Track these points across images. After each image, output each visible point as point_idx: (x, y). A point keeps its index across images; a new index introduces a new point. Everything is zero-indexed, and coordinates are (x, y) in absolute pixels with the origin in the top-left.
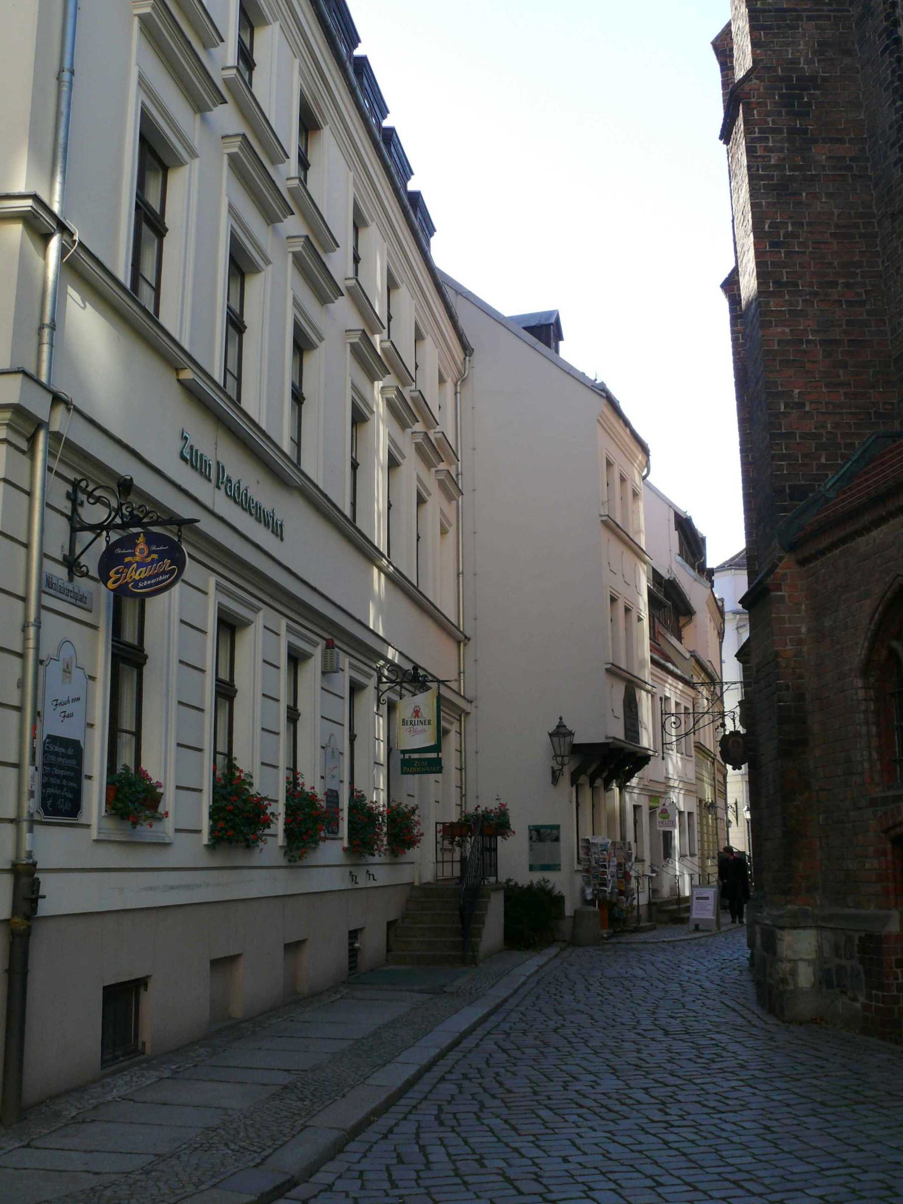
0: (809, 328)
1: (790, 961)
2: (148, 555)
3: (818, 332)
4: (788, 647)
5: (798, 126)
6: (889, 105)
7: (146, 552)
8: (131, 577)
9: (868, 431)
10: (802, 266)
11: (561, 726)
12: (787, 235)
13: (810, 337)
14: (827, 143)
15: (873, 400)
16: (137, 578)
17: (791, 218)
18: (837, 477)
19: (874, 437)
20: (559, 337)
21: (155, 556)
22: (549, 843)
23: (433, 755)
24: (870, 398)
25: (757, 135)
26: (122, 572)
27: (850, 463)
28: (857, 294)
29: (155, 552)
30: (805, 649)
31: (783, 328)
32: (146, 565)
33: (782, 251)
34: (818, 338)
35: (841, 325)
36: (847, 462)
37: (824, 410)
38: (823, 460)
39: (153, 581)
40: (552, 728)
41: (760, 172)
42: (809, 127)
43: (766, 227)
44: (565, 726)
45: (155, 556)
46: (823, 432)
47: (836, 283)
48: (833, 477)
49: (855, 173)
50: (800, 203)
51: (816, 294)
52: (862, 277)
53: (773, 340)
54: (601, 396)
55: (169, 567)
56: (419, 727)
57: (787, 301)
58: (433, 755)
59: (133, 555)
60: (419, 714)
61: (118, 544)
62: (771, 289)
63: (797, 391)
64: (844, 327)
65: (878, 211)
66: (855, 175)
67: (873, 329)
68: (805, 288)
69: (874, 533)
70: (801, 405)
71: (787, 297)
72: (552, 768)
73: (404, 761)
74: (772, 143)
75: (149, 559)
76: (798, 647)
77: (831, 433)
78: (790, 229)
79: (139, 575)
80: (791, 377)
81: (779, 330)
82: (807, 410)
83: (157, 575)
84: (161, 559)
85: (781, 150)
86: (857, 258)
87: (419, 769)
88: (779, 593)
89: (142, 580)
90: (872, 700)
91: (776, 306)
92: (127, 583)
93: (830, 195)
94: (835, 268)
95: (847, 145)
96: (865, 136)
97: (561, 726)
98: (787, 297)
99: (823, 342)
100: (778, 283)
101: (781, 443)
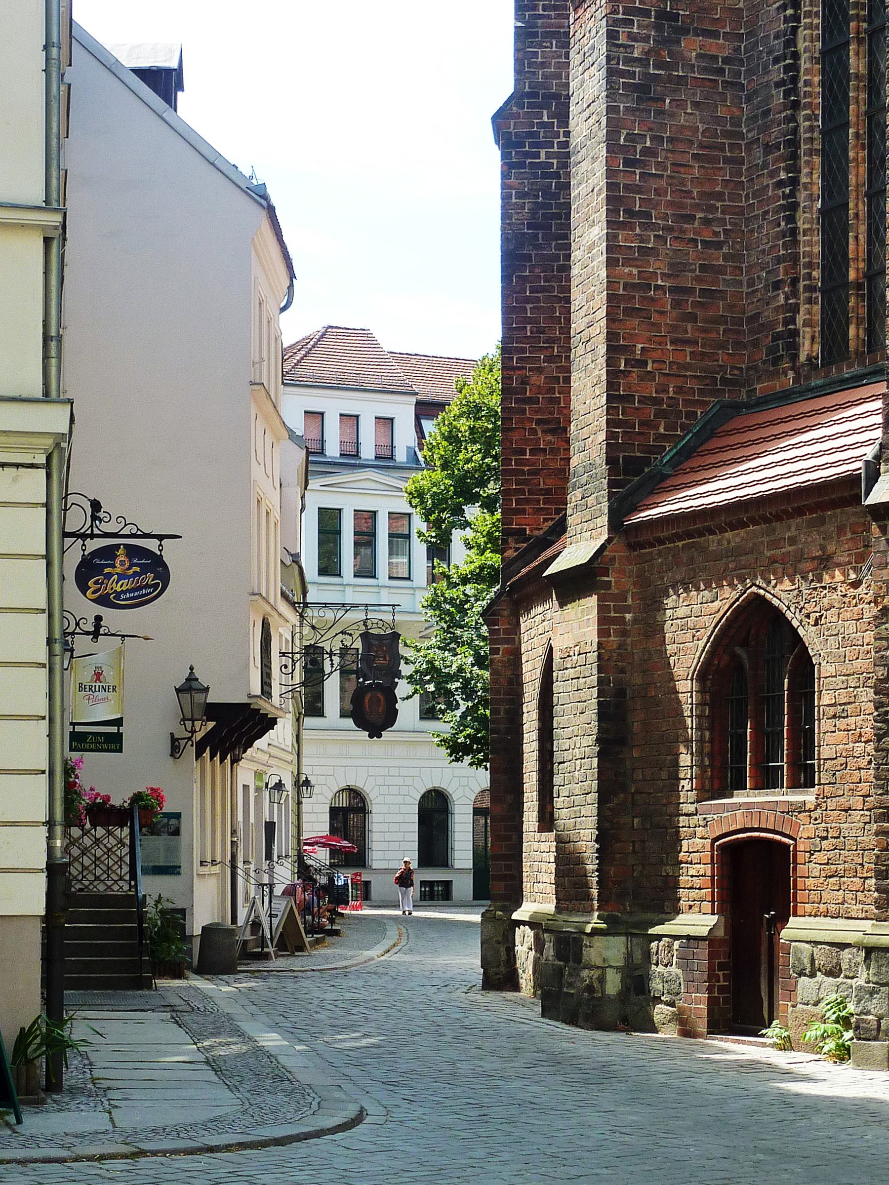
0: (659, 271)
1: (598, 967)
2: (129, 568)
3: (668, 276)
4: (612, 638)
5: (668, 9)
6: (778, 8)
7: (127, 564)
8: (112, 589)
9: (712, 399)
10: (658, 192)
11: (191, 679)
12: (646, 151)
13: (659, 282)
14: (699, 36)
15: (720, 363)
16: (119, 590)
17: (651, 130)
18: (675, 451)
19: (718, 407)
20: (180, 86)
21: (138, 569)
22: (165, 837)
23: (114, 729)
24: (718, 361)
25: (620, 16)
26: (102, 583)
27: (691, 435)
28: (716, 234)
29: (137, 565)
30: (629, 640)
31: (631, 269)
32: (129, 577)
33: (638, 171)
34: (668, 284)
35: (694, 271)
36: (687, 434)
37: (667, 372)
38: (662, 430)
39: (136, 594)
40: (180, 681)
41: (621, 67)
42: (681, 12)
43: (622, 140)
44: (197, 679)
45: (138, 569)
46: (664, 396)
47: (692, 218)
48: (670, 451)
49: (726, 78)
50: (663, 112)
51: (670, 229)
52: (723, 212)
53: (619, 282)
54: (261, 205)
55: (152, 581)
56: (101, 695)
57: (638, 235)
58: (114, 729)
59: (113, 566)
60: (102, 678)
61: (97, 553)
62: (621, 219)
63: (640, 346)
64: (697, 272)
65: (748, 132)
66: (727, 82)
67: (728, 277)
68: (659, 222)
69: (729, 535)
70: (643, 363)
71: (638, 231)
72: (172, 734)
73: (74, 736)
74: (638, 28)
75: (131, 572)
76: (623, 639)
77: (672, 398)
78: (648, 144)
79: (121, 587)
80: (635, 329)
81: (626, 270)
82: (648, 369)
83: (140, 588)
84: (144, 571)
85: (646, 39)
86: (718, 189)
87: (93, 746)
88: (606, 579)
89: (128, 591)
90: (707, 704)
91: (625, 240)
92: (108, 594)
93: (696, 105)
94: (693, 198)
95: (721, 41)
96: (742, 31)
97: (191, 679)
98: (638, 231)
99: (672, 290)
100: (629, 212)
101: (619, 407)
